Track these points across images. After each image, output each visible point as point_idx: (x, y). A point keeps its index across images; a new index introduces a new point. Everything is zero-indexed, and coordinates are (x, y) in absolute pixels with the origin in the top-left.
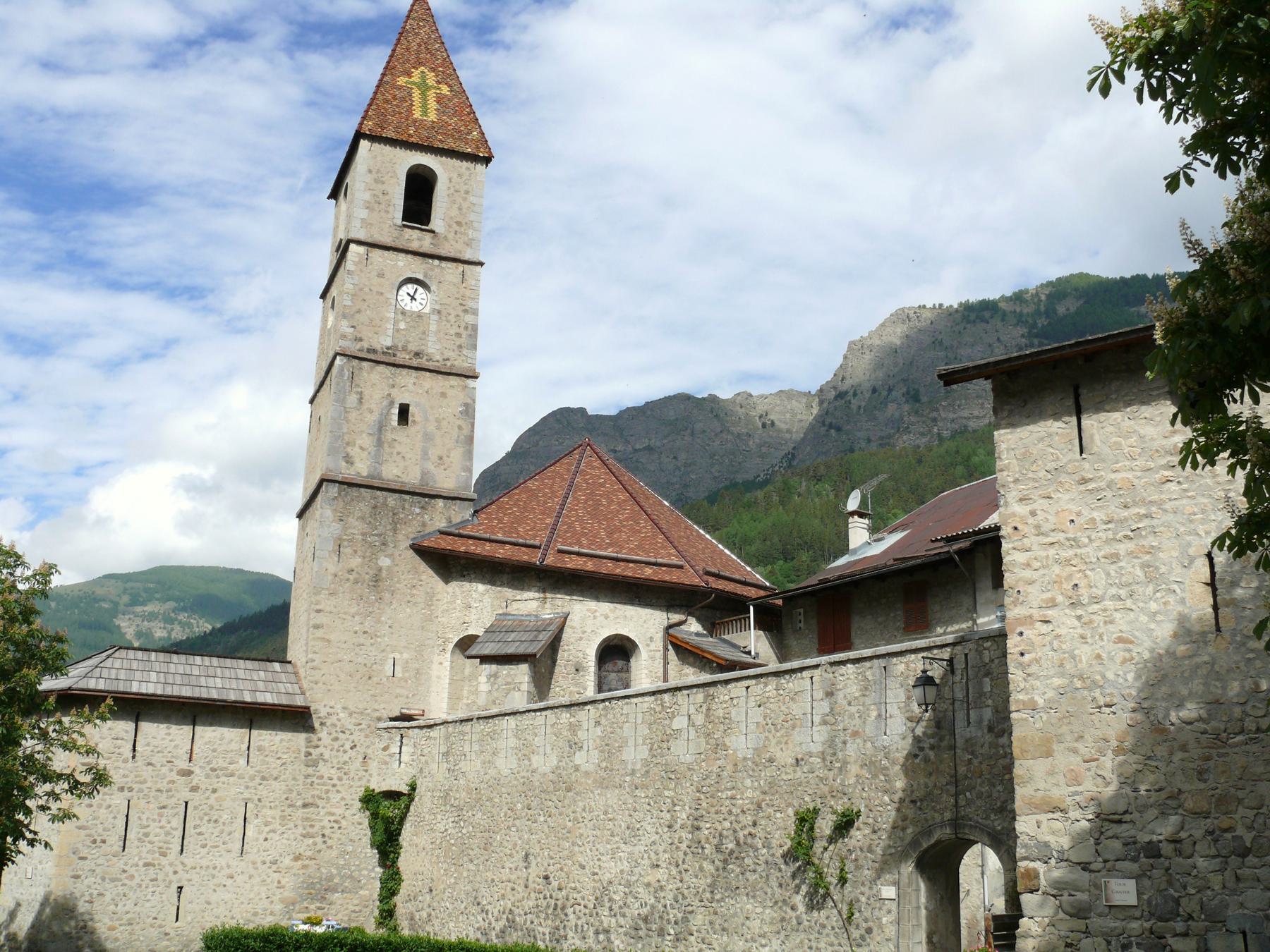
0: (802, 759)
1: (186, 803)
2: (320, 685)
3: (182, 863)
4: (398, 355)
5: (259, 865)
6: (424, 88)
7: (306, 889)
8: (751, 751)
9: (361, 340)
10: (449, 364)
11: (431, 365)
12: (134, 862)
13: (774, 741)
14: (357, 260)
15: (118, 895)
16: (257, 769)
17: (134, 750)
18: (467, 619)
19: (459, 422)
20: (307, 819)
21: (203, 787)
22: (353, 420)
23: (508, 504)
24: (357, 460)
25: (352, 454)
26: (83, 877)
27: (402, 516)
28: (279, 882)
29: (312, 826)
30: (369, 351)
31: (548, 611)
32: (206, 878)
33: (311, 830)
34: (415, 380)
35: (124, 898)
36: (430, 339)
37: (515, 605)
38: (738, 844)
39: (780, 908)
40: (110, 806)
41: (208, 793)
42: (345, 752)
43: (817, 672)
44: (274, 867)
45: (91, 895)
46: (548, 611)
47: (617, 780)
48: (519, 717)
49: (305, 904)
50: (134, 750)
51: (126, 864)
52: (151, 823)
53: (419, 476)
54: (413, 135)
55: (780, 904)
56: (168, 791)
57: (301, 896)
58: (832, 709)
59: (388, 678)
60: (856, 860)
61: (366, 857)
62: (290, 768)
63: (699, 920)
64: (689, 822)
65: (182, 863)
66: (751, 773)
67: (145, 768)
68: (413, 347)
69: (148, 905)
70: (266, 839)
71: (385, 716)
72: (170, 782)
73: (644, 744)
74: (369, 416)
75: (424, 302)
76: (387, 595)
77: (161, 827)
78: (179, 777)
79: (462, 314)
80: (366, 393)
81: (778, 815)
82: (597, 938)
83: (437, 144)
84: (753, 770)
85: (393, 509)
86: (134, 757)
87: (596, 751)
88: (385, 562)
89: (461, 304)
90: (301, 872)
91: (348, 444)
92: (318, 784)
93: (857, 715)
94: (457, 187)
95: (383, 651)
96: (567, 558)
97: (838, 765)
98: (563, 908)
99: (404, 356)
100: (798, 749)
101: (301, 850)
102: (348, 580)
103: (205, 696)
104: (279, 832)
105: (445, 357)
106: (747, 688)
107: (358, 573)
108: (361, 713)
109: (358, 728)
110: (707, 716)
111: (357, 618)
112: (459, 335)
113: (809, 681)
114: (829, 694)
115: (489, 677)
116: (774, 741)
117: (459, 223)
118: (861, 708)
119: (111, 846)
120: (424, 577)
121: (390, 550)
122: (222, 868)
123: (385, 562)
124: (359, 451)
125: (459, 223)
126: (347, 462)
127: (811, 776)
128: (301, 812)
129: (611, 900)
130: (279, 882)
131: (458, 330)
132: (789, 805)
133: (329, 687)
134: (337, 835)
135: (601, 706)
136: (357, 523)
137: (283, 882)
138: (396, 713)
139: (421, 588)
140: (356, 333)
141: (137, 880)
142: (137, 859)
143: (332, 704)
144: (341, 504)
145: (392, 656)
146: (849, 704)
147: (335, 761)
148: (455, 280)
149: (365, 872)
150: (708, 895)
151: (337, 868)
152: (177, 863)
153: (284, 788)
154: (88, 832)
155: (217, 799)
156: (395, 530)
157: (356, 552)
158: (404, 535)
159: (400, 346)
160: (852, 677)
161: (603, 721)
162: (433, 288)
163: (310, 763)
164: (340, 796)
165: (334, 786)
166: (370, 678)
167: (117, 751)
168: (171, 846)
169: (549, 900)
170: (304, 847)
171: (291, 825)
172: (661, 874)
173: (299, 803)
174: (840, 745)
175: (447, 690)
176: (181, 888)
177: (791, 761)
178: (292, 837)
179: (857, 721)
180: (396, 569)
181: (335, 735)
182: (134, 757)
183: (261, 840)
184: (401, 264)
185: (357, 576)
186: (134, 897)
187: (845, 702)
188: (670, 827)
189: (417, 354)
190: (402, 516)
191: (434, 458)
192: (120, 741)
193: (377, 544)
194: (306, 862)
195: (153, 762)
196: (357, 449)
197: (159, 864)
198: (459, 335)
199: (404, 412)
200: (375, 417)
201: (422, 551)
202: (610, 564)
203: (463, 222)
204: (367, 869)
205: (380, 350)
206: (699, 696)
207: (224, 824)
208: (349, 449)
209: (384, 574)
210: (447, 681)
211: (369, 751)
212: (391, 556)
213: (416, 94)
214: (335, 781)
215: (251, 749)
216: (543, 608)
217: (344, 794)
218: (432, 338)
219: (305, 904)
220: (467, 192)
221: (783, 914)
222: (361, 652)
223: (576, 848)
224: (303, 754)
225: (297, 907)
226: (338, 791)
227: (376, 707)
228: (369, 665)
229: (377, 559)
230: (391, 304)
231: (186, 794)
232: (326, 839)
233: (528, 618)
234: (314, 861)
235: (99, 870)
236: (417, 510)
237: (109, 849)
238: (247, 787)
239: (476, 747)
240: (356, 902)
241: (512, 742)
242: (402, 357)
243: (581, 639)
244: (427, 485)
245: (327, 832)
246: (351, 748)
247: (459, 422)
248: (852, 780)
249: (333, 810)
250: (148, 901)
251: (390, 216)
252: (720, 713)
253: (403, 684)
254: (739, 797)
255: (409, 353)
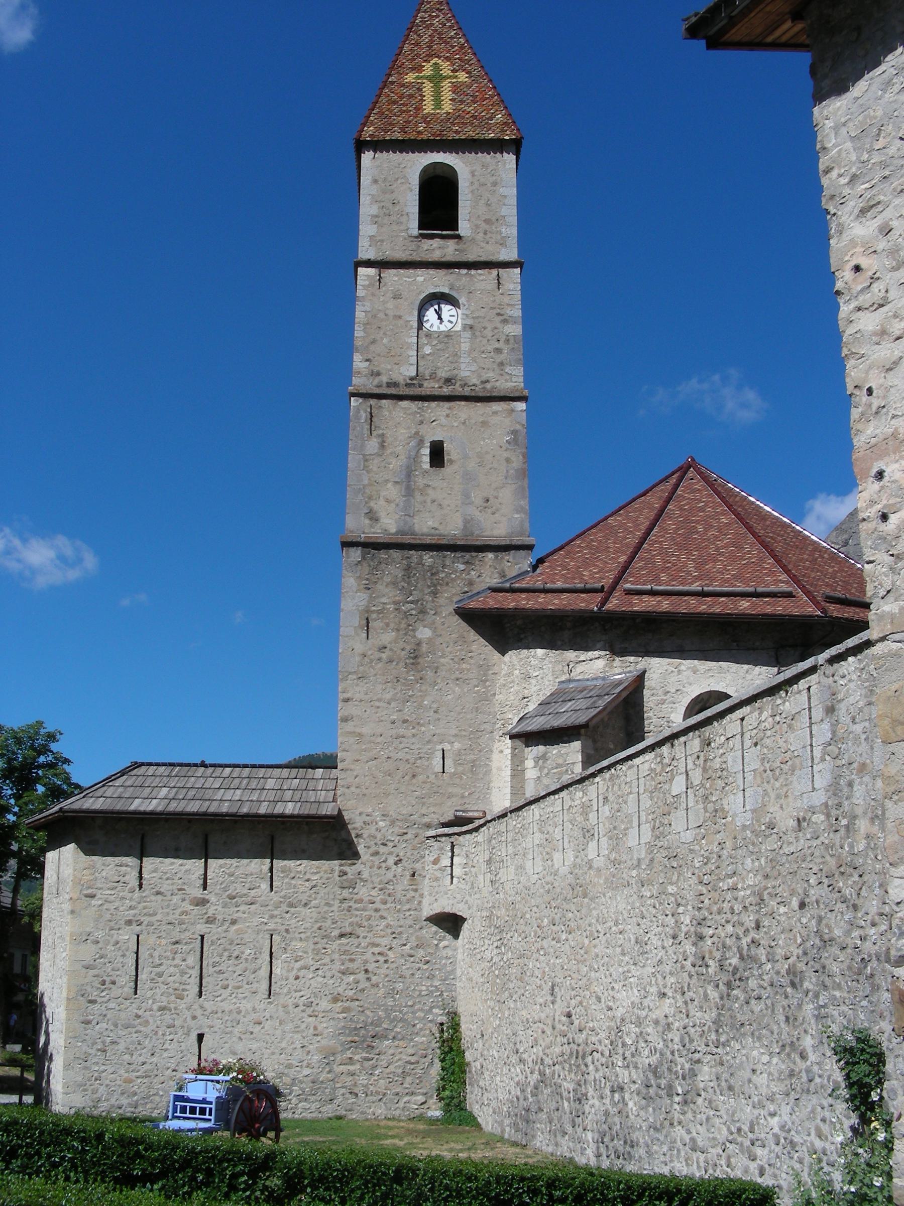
0: (804, 819)
1: (202, 937)
2: (353, 789)
3: (202, 1007)
4: (426, 384)
5: (291, 1008)
6: (437, 79)
7: (348, 1036)
8: (749, 815)
9: (378, 374)
10: (488, 386)
11: (467, 391)
12: (149, 1007)
13: (773, 795)
14: (367, 283)
15: (132, 1043)
16: (282, 894)
17: (141, 878)
18: (526, 693)
19: (506, 455)
20: (345, 952)
21: (220, 917)
22: (375, 469)
23: (579, 546)
24: (382, 515)
25: (375, 507)
26: (94, 1023)
27: (443, 575)
28: (315, 1028)
29: (352, 960)
30: (389, 385)
31: (617, 671)
32: (229, 1024)
33: (351, 965)
34: (448, 412)
35: (139, 1047)
36: (462, 360)
37: (580, 668)
38: (742, 958)
39: (789, 1055)
40: (117, 943)
41: (227, 924)
42: (388, 869)
43: (814, 678)
44: (309, 1011)
45: (104, 1042)
46: (617, 671)
47: (624, 875)
48: (542, 804)
49: (349, 1054)
50: (141, 878)
51: (139, 1008)
52: (164, 961)
53: (460, 525)
54: (424, 131)
55: (788, 1049)
56: (181, 923)
57: (342, 1044)
58: (834, 733)
59: (436, 774)
60: (872, 976)
61: (420, 995)
62: (322, 892)
63: (706, 1073)
64: (693, 929)
65: (202, 1007)
66: (751, 848)
67: (153, 898)
68: (443, 374)
69: (166, 1054)
70: (297, 978)
71: (436, 822)
72: (182, 913)
73: (647, 822)
74: (394, 461)
75: (454, 319)
76: (430, 674)
77: (175, 966)
78: (192, 908)
79: (499, 325)
80: (388, 433)
81: (782, 910)
82: (613, 1097)
83: (452, 136)
84: (753, 844)
85: (431, 567)
86: (141, 886)
87: (605, 838)
88: (424, 633)
89: (499, 314)
90: (341, 1016)
91: (370, 498)
92: (357, 909)
93: (863, 737)
94: (482, 180)
95: (429, 742)
96: (635, 599)
97: (844, 822)
98: (583, 1057)
99: (432, 384)
100: (799, 804)
101: (340, 990)
102: (380, 659)
103: (212, 810)
104: (312, 968)
105: (484, 379)
106: (742, 719)
107: (391, 650)
108: (406, 821)
109: (402, 838)
110: (705, 770)
111: (393, 704)
112: (498, 351)
113: (805, 693)
114: (830, 710)
115: (537, 759)
116: (773, 795)
117: (487, 221)
118: (867, 724)
119: (122, 987)
120: (474, 647)
121: (429, 619)
122: (247, 1012)
123: (424, 633)
124: (384, 503)
125: (487, 221)
126: (371, 519)
127: (815, 843)
128: (335, 945)
129: (624, 1045)
130: (315, 1028)
131: (497, 345)
132: (793, 893)
133: (365, 791)
134: (383, 971)
135: (607, 775)
136: (387, 590)
137: (320, 1028)
138: (449, 816)
139: (472, 661)
140: (372, 367)
141: (152, 1027)
142: (150, 1002)
143: (370, 810)
144: (366, 570)
145: (440, 747)
146: (853, 721)
147: (376, 880)
148: (489, 287)
149: (420, 1014)
150: (713, 1036)
151: (386, 1010)
152: (196, 1006)
153: (315, 915)
154: (95, 972)
155: (236, 931)
156: (435, 594)
157: (387, 625)
158: (447, 598)
159: (427, 374)
160: (854, 677)
161: (611, 798)
162: (462, 300)
163: (346, 884)
164: (384, 923)
165: (376, 910)
166: (414, 776)
167: (123, 879)
168: (187, 987)
169: (572, 1045)
170: (344, 986)
171: (327, 960)
172: (667, 1007)
173: (336, 933)
174: (846, 789)
175: (509, 784)
176: (200, 1037)
177: (792, 823)
178: (329, 974)
179: (864, 747)
180: (440, 640)
181: (374, 849)
182: (141, 886)
183: (292, 980)
184: (420, 279)
185: (390, 653)
186: (150, 1046)
187: (848, 720)
188: (674, 937)
189: (448, 381)
190: (442, 575)
191: (478, 500)
192: (124, 868)
193: (414, 612)
194: (347, 1004)
195: (162, 890)
196: (382, 502)
197: (176, 1009)
198: (498, 351)
199: (438, 455)
200: (402, 460)
201: (469, 616)
202: (693, 601)
203: (494, 219)
204: (422, 1010)
205: (402, 382)
206: (694, 742)
207: (246, 959)
208: (372, 504)
209: (424, 648)
210: (509, 773)
211: (418, 866)
212: (432, 626)
213: (428, 88)
214: (378, 905)
215: (274, 871)
216: (612, 667)
217: (390, 920)
218: (464, 359)
219: (349, 1054)
220: (495, 184)
221: (792, 1065)
222: (402, 746)
223: (593, 974)
224: (337, 873)
225: (339, 1058)
226: (382, 917)
227: (424, 811)
228: (412, 761)
229: (414, 630)
230: (412, 327)
231: (201, 928)
232: (370, 975)
233: (595, 682)
234: (357, 1003)
235: (110, 1015)
236: (462, 567)
237: (120, 991)
238: (272, 917)
239: (511, 850)
240: (411, 1051)
241: (538, 838)
242: (430, 387)
243: (663, 702)
244: (472, 534)
245: (371, 967)
246: (396, 864)
247: (506, 455)
248: (861, 846)
249: (378, 940)
250: (166, 1050)
251: (403, 227)
252: (717, 764)
253: (457, 781)
254: (739, 886)
255: (438, 381)
